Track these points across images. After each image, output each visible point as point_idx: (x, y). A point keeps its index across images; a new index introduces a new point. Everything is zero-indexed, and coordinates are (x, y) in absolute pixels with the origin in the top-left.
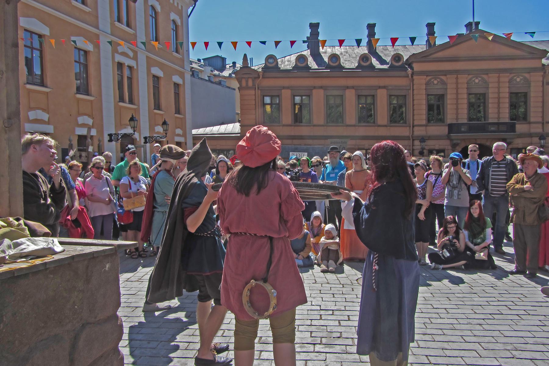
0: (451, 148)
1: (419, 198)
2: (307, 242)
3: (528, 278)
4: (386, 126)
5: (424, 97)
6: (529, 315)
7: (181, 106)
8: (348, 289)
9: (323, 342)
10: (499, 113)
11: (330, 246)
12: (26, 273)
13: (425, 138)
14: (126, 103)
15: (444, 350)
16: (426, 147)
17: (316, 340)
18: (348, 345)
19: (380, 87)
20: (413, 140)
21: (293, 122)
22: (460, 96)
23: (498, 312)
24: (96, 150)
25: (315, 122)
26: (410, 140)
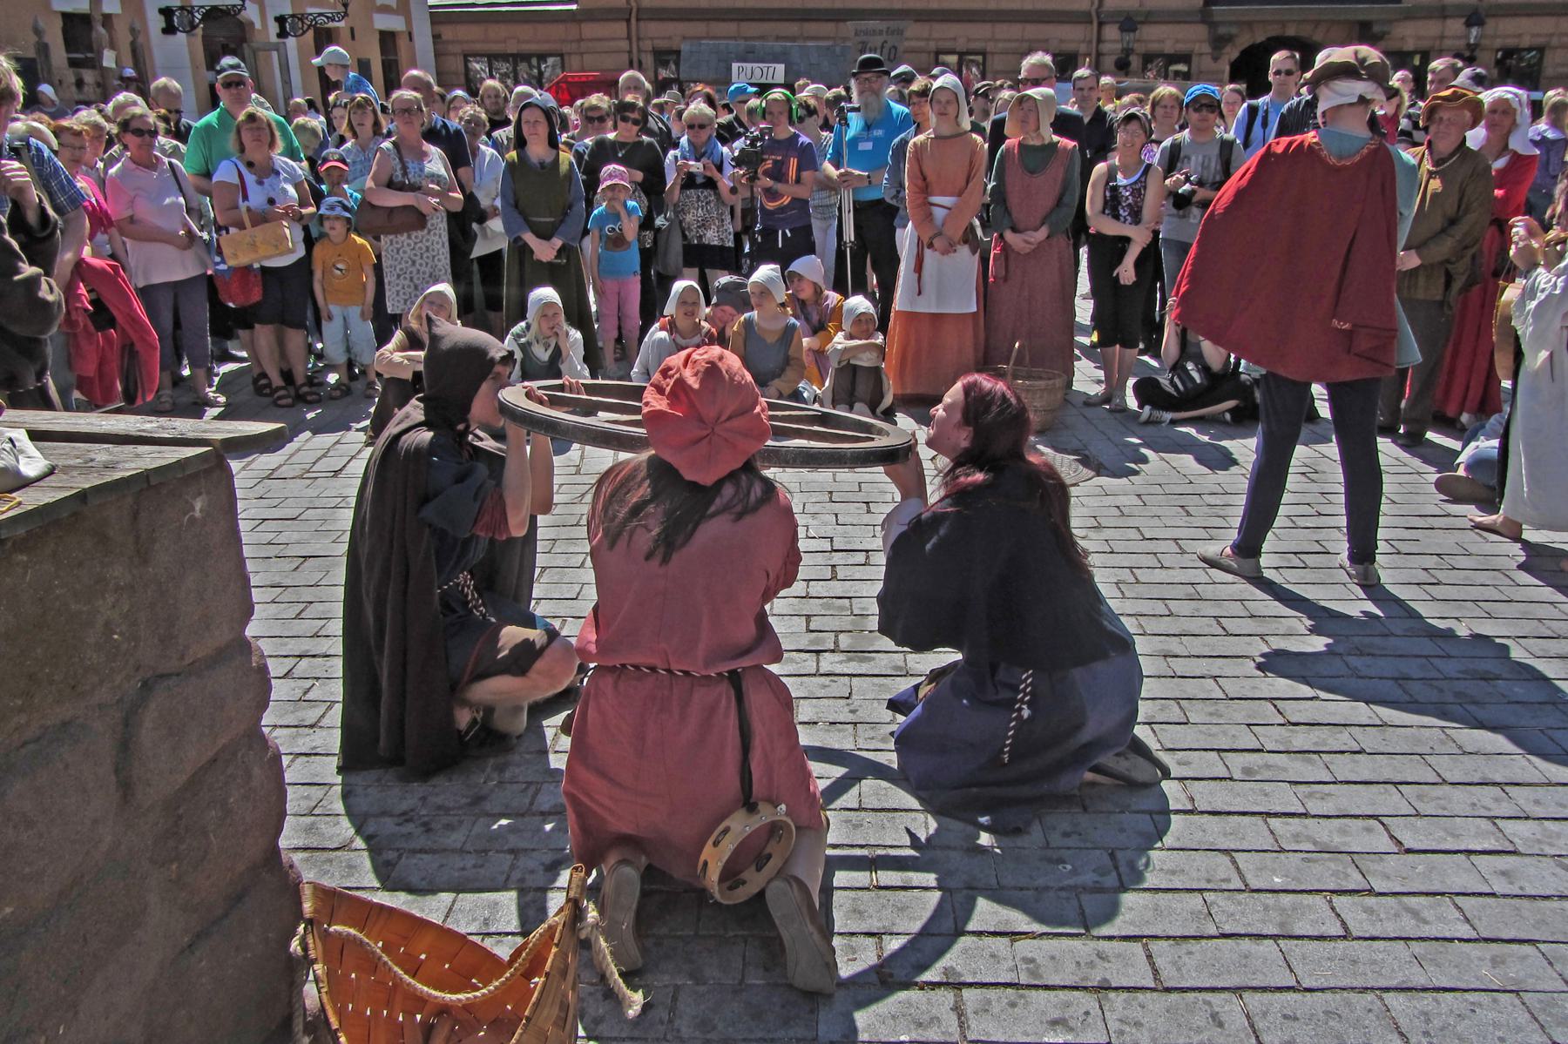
2: (791, 352)
3: (1404, 447)
6: (1399, 553)
9: (843, 646)
11: (854, 357)
15: (1169, 659)
16: (1136, 46)
17: (823, 641)
20: (1101, 24)
23: (1318, 548)
24: (127, 58)
26: (1091, 22)
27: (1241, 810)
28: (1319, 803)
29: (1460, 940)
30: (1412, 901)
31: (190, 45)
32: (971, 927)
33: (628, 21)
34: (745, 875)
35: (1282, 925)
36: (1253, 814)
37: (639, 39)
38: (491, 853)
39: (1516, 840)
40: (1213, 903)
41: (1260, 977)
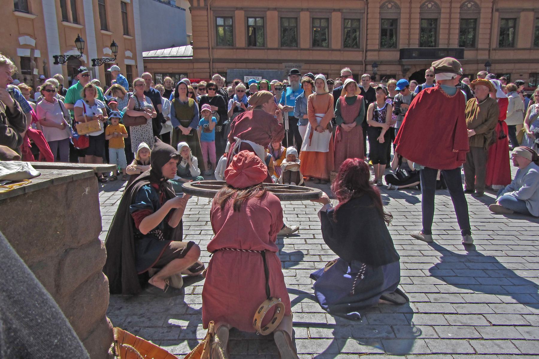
0: (402, 74)
1: (379, 121)
4: (339, 50)
5: (378, 21)
6: (479, 230)
7: (130, 26)
8: (311, 209)
10: (449, 39)
12: (5, 198)
13: (377, 63)
14: (70, 22)
18: (316, 262)
19: (334, 10)
20: (366, 65)
21: (247, 45)
22: (412, 21)
23: (451, 228)
24: (42, 72)
25: (269, 45)
26: (363, 64)
27: (435, 312)
28: (461, 310)
29: (515, 354)
30: (497, 341)
31: (63, 68)
32: (343, 350)
33: (209, 62)
34: (268, 326)
35: (453, 350)
36: (439, 313)
37: (213, 68)
38: (173, 328)
39: (530, 321)
40: (428, 343)
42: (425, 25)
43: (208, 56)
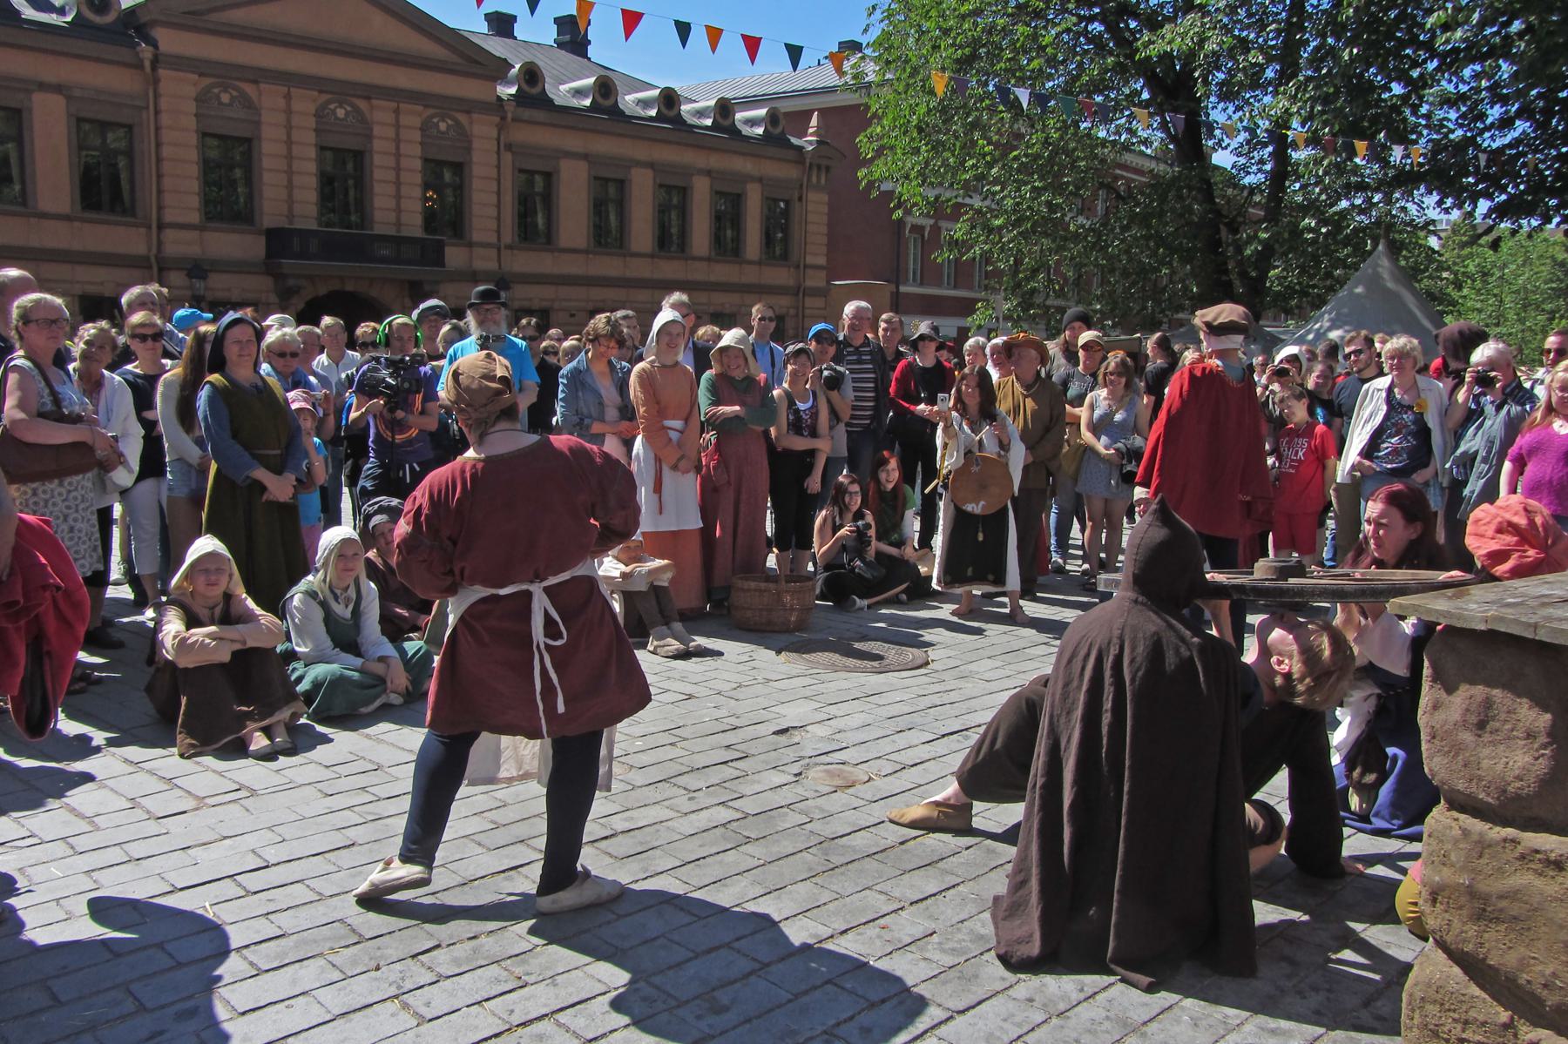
5: (193, 139)
41: (506, 861)
42: (213, 154)
43: (497, 265)
